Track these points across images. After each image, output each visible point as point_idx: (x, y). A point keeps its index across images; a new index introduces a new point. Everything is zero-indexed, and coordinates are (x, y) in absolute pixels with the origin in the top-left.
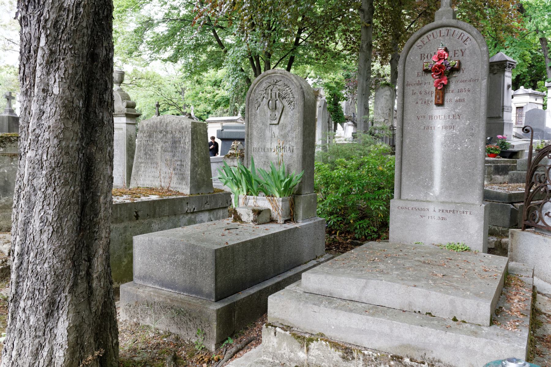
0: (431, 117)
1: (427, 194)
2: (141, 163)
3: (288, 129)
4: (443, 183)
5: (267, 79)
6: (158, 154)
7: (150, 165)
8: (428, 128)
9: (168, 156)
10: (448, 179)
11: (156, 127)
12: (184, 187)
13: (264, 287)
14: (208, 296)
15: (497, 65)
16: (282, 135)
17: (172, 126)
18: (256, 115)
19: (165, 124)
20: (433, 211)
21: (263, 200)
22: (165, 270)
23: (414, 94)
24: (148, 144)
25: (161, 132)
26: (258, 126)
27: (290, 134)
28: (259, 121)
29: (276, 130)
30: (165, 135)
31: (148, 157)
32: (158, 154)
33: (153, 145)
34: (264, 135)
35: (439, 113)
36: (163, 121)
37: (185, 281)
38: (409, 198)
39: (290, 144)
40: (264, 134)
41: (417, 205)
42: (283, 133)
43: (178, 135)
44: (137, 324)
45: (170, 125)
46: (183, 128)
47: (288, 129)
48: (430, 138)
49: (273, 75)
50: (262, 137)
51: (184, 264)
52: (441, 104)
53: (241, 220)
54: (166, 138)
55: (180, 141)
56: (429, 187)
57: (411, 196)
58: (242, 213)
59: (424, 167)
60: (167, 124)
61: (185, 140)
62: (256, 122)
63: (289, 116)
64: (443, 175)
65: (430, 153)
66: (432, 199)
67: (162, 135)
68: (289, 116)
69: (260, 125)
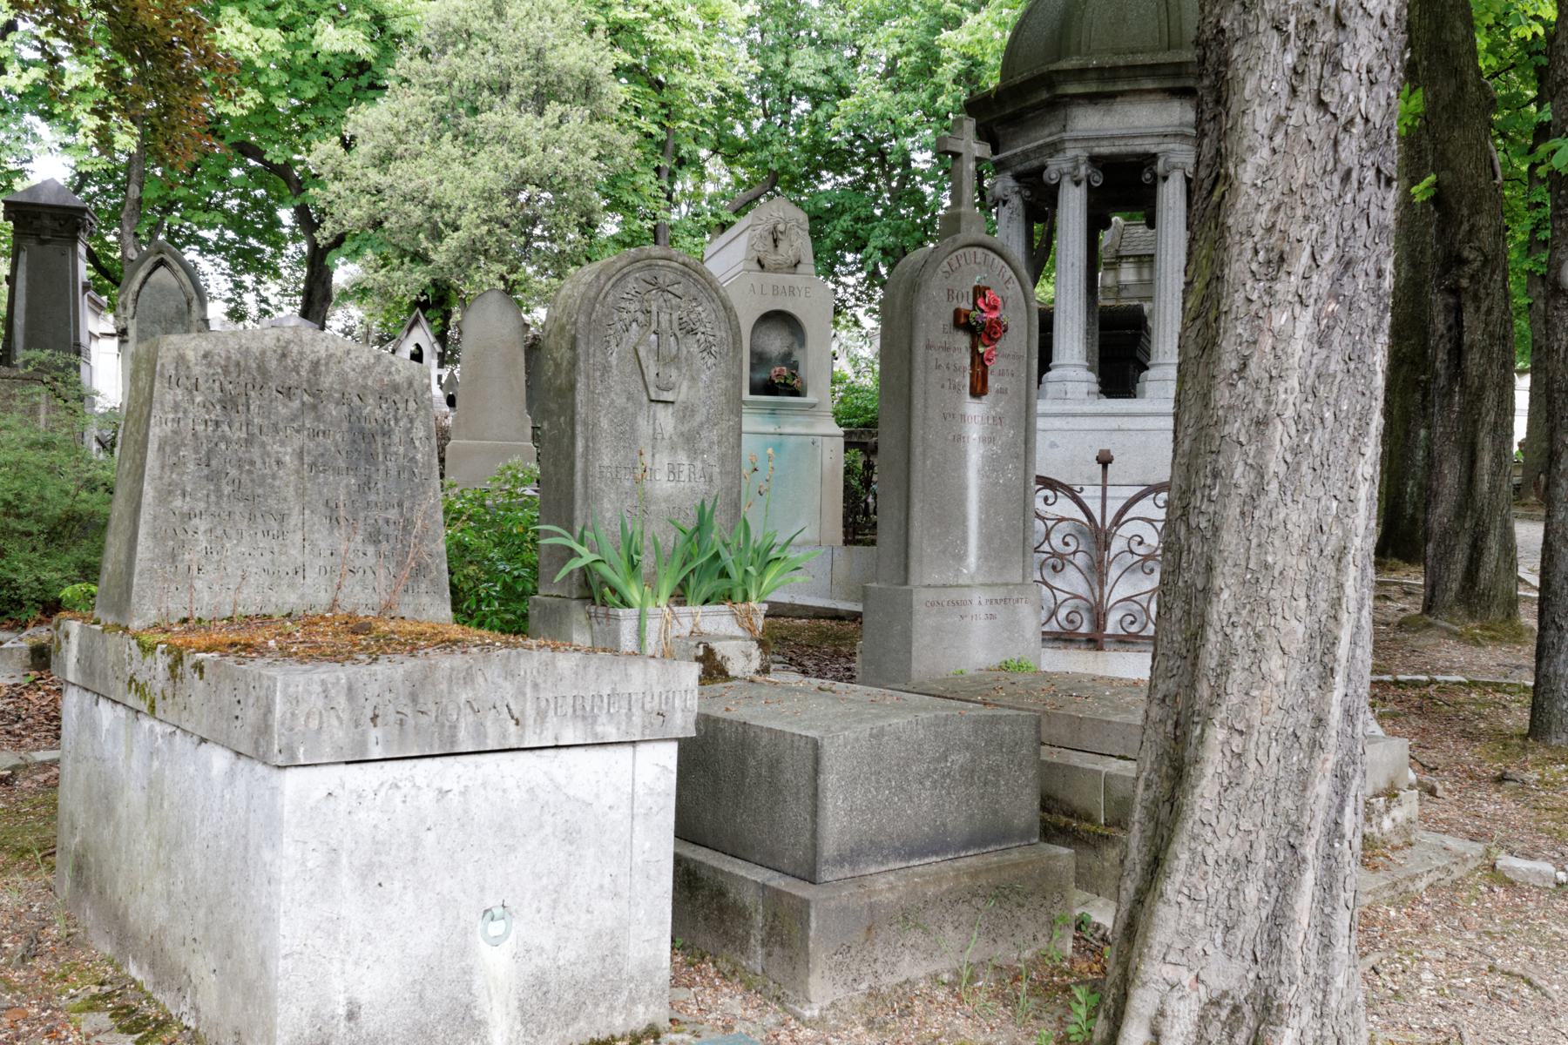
0: (963, 417)
1: (958, 572)
2: (189, 516)
3: (699, 418)
4: (981, 548)
5: (640, 269)
6: (287, 480)
7: (244, 525)
8: (959, 438)
9: (343, 486)
10: (987, 539)
11: (262, 369)
12: (425, 600)
13: (715, 863)
14: (1025, 835)
15: (53, 218)
16: (682, 434)
17: (342, 376)
18: (606, 369)
19: (306, 364)
20: (979, 601)
21: (718, 614)
22: (922, 807)
23: (938, 367)
24: (224, 438)
25: (287, 392)
26: (612, 402)
27: (704, 433)
28: (618, 388)
29: (666, 419)
30: (314, 407)
31: (227, 490)
32: (287, 480)
33: (249, 441)
34: (633, 430)
35: (975, 409)
36: (295, 349)
37: (971, 816)
38: (932, 582)
39: (703, 461)
40: (632, 427)
41: (946, 596)
42: (685, 428)
43: (372, 409)
44: (873, 994)
45: (335, 369)
46: (396, 388)
47: (699, 418)
48: (962, 457)
49: (661, 262)
50: (626, 435)
51: (969, 773)
52: (979, 389)
53: (727, 675)
54: (319, 418)
55: (387, 434)
56: (961, 557)
57: (936, 578)
58: (727, 654)
59: (952, 518)
60: (316, 365)
61: (408, 431)
62: (609, 389)
63: (701, 385)
64: (980, 533)
65: (962, 488)
66: (968, 582)
67: (296, 404)
68: (701, 385)
69: (621, 401)
